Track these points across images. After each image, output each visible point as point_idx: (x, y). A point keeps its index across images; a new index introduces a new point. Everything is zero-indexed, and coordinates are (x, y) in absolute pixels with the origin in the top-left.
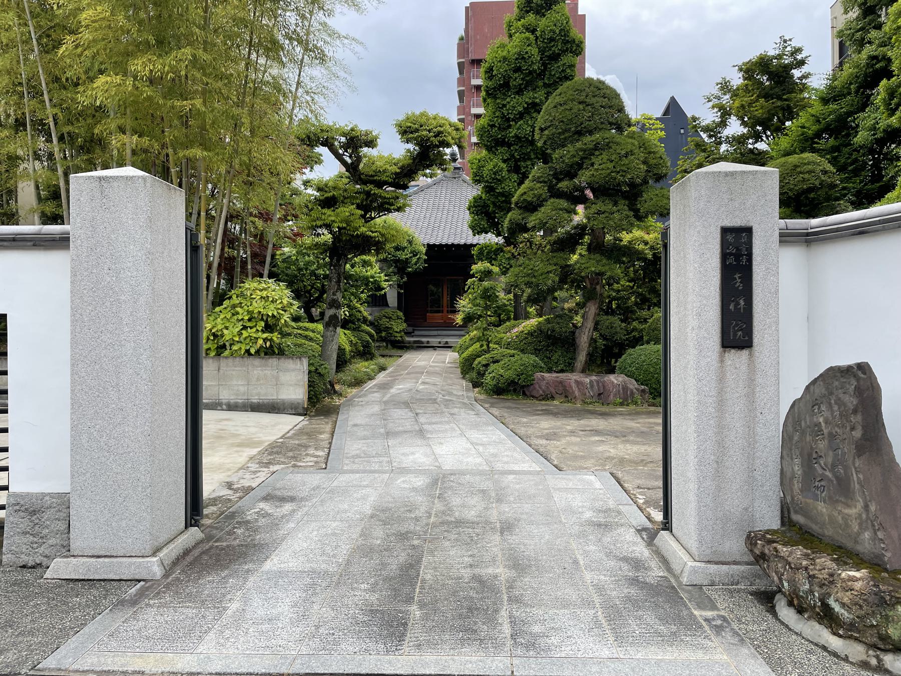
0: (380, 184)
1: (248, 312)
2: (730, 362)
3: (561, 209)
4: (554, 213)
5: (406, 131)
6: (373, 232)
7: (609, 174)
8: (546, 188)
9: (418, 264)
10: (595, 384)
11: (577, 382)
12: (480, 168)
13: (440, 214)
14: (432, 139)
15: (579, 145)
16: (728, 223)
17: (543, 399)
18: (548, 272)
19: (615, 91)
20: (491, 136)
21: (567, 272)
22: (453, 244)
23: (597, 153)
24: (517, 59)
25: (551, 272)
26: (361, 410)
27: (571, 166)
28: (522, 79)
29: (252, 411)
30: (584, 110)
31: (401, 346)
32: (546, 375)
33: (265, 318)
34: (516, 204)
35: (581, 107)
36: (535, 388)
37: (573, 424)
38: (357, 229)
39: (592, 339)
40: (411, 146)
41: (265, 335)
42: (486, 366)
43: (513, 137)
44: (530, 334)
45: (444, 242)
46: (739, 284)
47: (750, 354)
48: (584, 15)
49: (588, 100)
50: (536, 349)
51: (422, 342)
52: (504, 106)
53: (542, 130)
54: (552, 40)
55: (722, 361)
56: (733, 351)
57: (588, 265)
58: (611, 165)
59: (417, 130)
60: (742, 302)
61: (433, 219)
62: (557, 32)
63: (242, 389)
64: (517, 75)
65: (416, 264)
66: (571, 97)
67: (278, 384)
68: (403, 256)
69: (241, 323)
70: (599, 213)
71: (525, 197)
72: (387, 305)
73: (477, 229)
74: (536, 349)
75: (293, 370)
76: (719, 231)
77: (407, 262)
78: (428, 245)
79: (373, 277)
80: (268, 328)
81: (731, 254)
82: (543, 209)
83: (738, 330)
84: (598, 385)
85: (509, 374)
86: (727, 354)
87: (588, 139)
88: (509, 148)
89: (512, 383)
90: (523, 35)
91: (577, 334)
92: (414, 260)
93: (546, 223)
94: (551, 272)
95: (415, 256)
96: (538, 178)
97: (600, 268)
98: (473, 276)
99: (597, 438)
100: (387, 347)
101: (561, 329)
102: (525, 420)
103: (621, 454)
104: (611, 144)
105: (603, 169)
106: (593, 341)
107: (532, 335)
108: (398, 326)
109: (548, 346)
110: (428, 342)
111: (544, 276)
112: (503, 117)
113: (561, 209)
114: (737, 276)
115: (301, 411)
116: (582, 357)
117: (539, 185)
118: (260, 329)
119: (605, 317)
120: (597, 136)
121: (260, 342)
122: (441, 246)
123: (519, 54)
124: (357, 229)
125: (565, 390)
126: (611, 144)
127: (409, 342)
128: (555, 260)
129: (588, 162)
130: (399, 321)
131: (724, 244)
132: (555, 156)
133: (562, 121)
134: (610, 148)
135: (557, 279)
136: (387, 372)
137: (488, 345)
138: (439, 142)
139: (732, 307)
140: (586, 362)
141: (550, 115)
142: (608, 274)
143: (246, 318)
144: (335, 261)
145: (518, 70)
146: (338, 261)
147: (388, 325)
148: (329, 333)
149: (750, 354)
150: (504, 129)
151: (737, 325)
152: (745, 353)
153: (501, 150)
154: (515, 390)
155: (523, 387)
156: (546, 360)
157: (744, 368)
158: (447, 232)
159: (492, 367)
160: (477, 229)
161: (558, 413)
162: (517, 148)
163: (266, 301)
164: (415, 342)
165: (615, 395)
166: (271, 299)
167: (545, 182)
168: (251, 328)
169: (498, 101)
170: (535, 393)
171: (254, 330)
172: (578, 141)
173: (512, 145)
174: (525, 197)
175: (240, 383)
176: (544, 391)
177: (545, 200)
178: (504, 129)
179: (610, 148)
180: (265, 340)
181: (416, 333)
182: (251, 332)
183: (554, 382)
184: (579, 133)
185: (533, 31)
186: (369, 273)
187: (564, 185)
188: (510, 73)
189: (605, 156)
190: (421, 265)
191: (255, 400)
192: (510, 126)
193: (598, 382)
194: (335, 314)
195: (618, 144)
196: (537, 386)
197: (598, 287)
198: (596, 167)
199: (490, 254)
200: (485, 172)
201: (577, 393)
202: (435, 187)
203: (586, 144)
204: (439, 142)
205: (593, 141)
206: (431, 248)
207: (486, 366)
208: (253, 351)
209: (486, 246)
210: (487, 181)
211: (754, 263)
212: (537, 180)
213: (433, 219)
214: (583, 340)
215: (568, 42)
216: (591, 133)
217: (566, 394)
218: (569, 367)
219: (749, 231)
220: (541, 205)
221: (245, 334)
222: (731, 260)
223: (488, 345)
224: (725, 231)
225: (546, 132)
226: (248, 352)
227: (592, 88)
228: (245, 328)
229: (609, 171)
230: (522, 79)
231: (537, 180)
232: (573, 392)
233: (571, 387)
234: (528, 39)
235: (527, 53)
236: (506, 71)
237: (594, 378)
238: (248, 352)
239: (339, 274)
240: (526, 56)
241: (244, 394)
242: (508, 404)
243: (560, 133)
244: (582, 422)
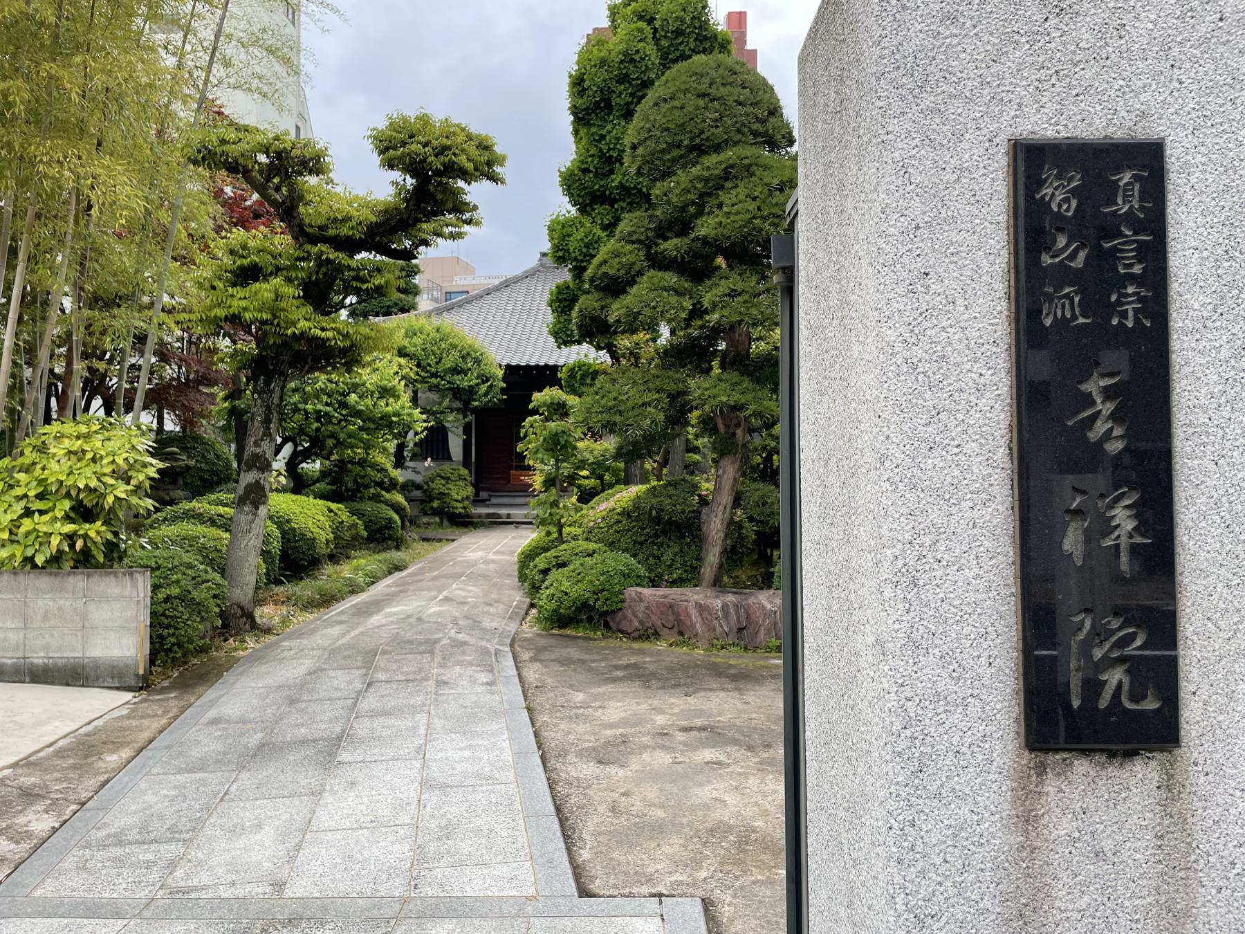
0: (351, 246)
1: (41, 482)
2: (1067, 826)
3: (665, 289)
4: (652, 295)
5: (394, 147)
6: (323, 329)
7: (750, 221)
8: (642, 253)
9: (492, 393)
10: (732, 610)
11: (701, 608)
12: (565, 236)
13: (531, 320)
14: (429, 159)
15: (696, 171)
16: (1045, 126)
17: (640, 637)
18: (644, 404)
19: (764, 79)
20: (585, 188)
21: (683, 406)
22: (546, 366)
23: (728, 185)
24: (622, 62)
25: (649, 404)
26: (291, 664)
27: (683, 209)
28: (632, 94)
29: (33, 682)
30: (706, 108)
31: (464, 522)
32: (647, 592)
33: (73, 493)
34: (592, 280)
35: (701, 103)
36: (625, 617)
37: (672, 707)
38: (294, 324)
39: (731, 521)
40: (396, 175)
41: (69, 528)
42: (545, 572)
43: (617, 188)
44: (626, 514)
45: (533, 362)
46: (1107, 431)
47: (1170, 786)
48: (755, 52)
49: (713, 91)
50: (635, 542)
51: (499, 516)
52: (603, 137)
53: (634, 147)
54: (678, 33)
55: (1027, 818)
56: (1082, 766)
57: (714, 391)
58: (752, 206)
59: (404, 144)
60: (1123, 520)
61: (520, 328)
62: (688, 20)
63: (14, 637)
64: (622, 87)
65: (486, 395)
66: (683, 87)
67: (85, 627)
68: (464, 382)
69: (23, 503)
70: (732, 294)
71: (604, 269)
72: (449, 458)
73: (563, 337)
74: (635, 542)
75: (118, 598)
76: (1001, 160)
77: (471, 390)
78: (508, 367)
79: (397, 414)
80: (83, 512)
81: (1063, 274)
82: (634, 290)
83: (1109, 663)
84: (737, 612)
85: (578, 591)
86: (1051, 785)
87: (712, 160)
88: (612, 206)
89: (585, 606)
90: (633, 26)
91: (703, 517)
92: (483, 388)
93: (639, 313)
94: (649, 404)
95: (484, 382)
96: (630, 235)
97: (736, 397)
98: (535, 412)
99: (708, 754)
100: (441, 524)
101: (673, 507)
102: (580, 697)
103: (748, 812)
104: (754, 168)
105: (738, 213)
106: (733, 527)
107: (629, 516)
108: (460, 492)
109: (657, 536)
110: (509, 516)
111: (636, 412)
112: (602, 155)
113: (665, 289)
114: (1094, 386)
115: (132, 682)
116: (713, 556)
117: (629, 247)
118: (60, 514)
119: (754, 486)
120: (729, 154)
121: (55, 541)
122: (537, 367)
123: (626, 54)
124: (294, 324)
125: (679, 621)
126: (754, 168)
127: (480, 516)
128: (658, 382)
129: (713, 201)
130: (462, 483)
131: (1032, 229)
132: (656, 192)
133: (667, 129)
134: (752, 174)
135: (661, 416)
136: (404, 573)
137: (560, 532)
138: (444, 165)
139: (1072, 542)
140: (721, 566)
141: (648, 120)
142: (752, 407)
143: (32, 494)
144: (261, 382)
145: (623, 79)
146: (268, 383)
147: (443, 490)
148: (242, 518)
149: (1170, 786)
150: (604, 175)
151: (1099, 634)
152: (1142, 775)
153: (599, 209)
154: (590, 619)
155: (605, 614)
156: (652, 561)
157: (1138, 851)
158: (539, 347)
159: (554, 575)
160: (563, 337)
161: (653, 675)
162: (624, 205)
163: (80, 460)
164: (488, 516)
165: (768, 632)
166: (89, 456)
167: (639, 241)
168: (41, 512)
169: (593, 130)
170: (625, 626)
171: (47, 517)
172: (694, 164)
173: (616, 201)
174: (604, 269)
175: (9, 624)
176: (641, 623)
177: (640, 274)
178: (604, 175)
179: (752, 174)
180: (71, 538)
181: (494, 501)
182: (42, 523)
183: (659, 605)
184: (700, 149)
185: (651, 21)
186: (389, 409)
187: (671, 246)
188: (613, 85)
189: (742, 190)
190: (497, 397)
191: (39, 658)
192: (612, 172)
193: (736, 606)
194: (257, 482)
195: (766, 167)
196: (629, 613)
197: (739, 432)
198: (725, 209)
199: (581, 377)
200: (573, 245)
201: (699, 627)
202: (527, 281)
203: (708, 168)
204: (444, 165)
205: (721, 163)
206: (511, 370)
207: (545, 572)
208: (40, 560)
209: (580, 365)
210: (575, 259)
211: (1178, 321)
212: (628, 238)
213: (520, 328)
214: (715, 526)
215: (706, 38)
216: (717, 149)
217: (682, 632)
218: (690, 577)
219: (1147, 158)
220: (632, 282)
221: (27, 524)
222: (1064, 307)
223: (560, 532)
224: (1032, 160)
225: (640, 151)
226: (29, 561)
227: (721, 71)
228: (28, 513)
229: (748, 216)
230: (632, 94)
231: (628, 238)
232: (693, 625)
233: (688, 615)
234: (640, 30)
235: (637, 52)
236: (605, 81)
237: (731, 598)
238: (29, 561)
239: (268, 408)
240: (637, 57)
241: (16, 648)
242: (573, 652)
243: (663, 151)
244: (691, 700)
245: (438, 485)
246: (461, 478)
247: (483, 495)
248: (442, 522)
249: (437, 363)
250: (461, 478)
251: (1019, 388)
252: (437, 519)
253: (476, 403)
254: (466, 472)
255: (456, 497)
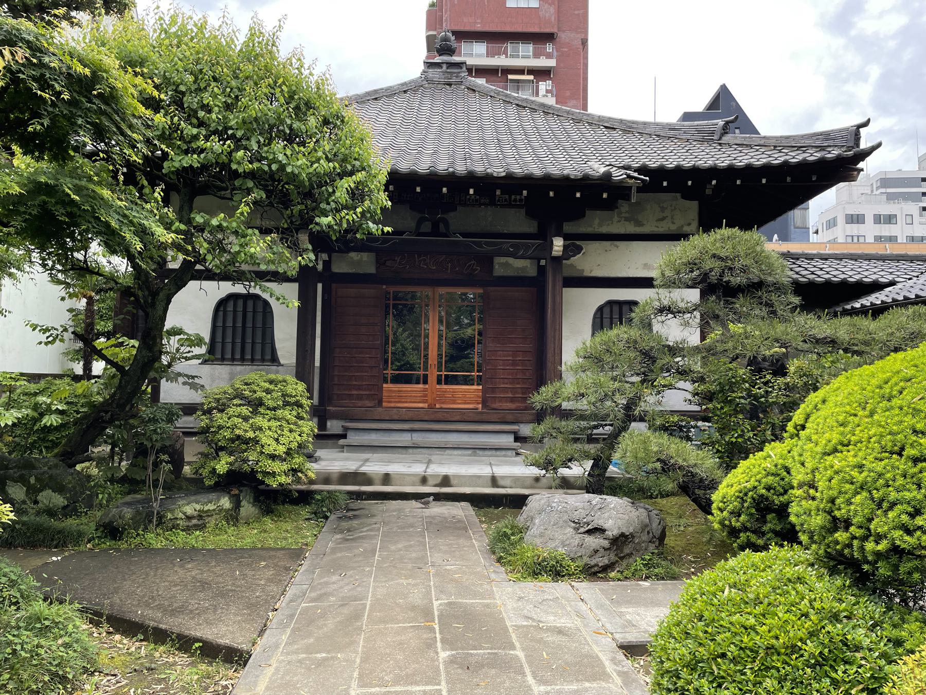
51: (366, 479)
100: (233, 517)
110: (386, 479)
130: (288, 414)
245: (234, 421)
246: (289, 402)
247: (334, 426)
248: (237, 505)
249: (228, 107)
250: (289, 402)
251: (200, 493)
252: (226, 502)
253: (325, 221)
254: (301, 387)
255: (272, 447)
